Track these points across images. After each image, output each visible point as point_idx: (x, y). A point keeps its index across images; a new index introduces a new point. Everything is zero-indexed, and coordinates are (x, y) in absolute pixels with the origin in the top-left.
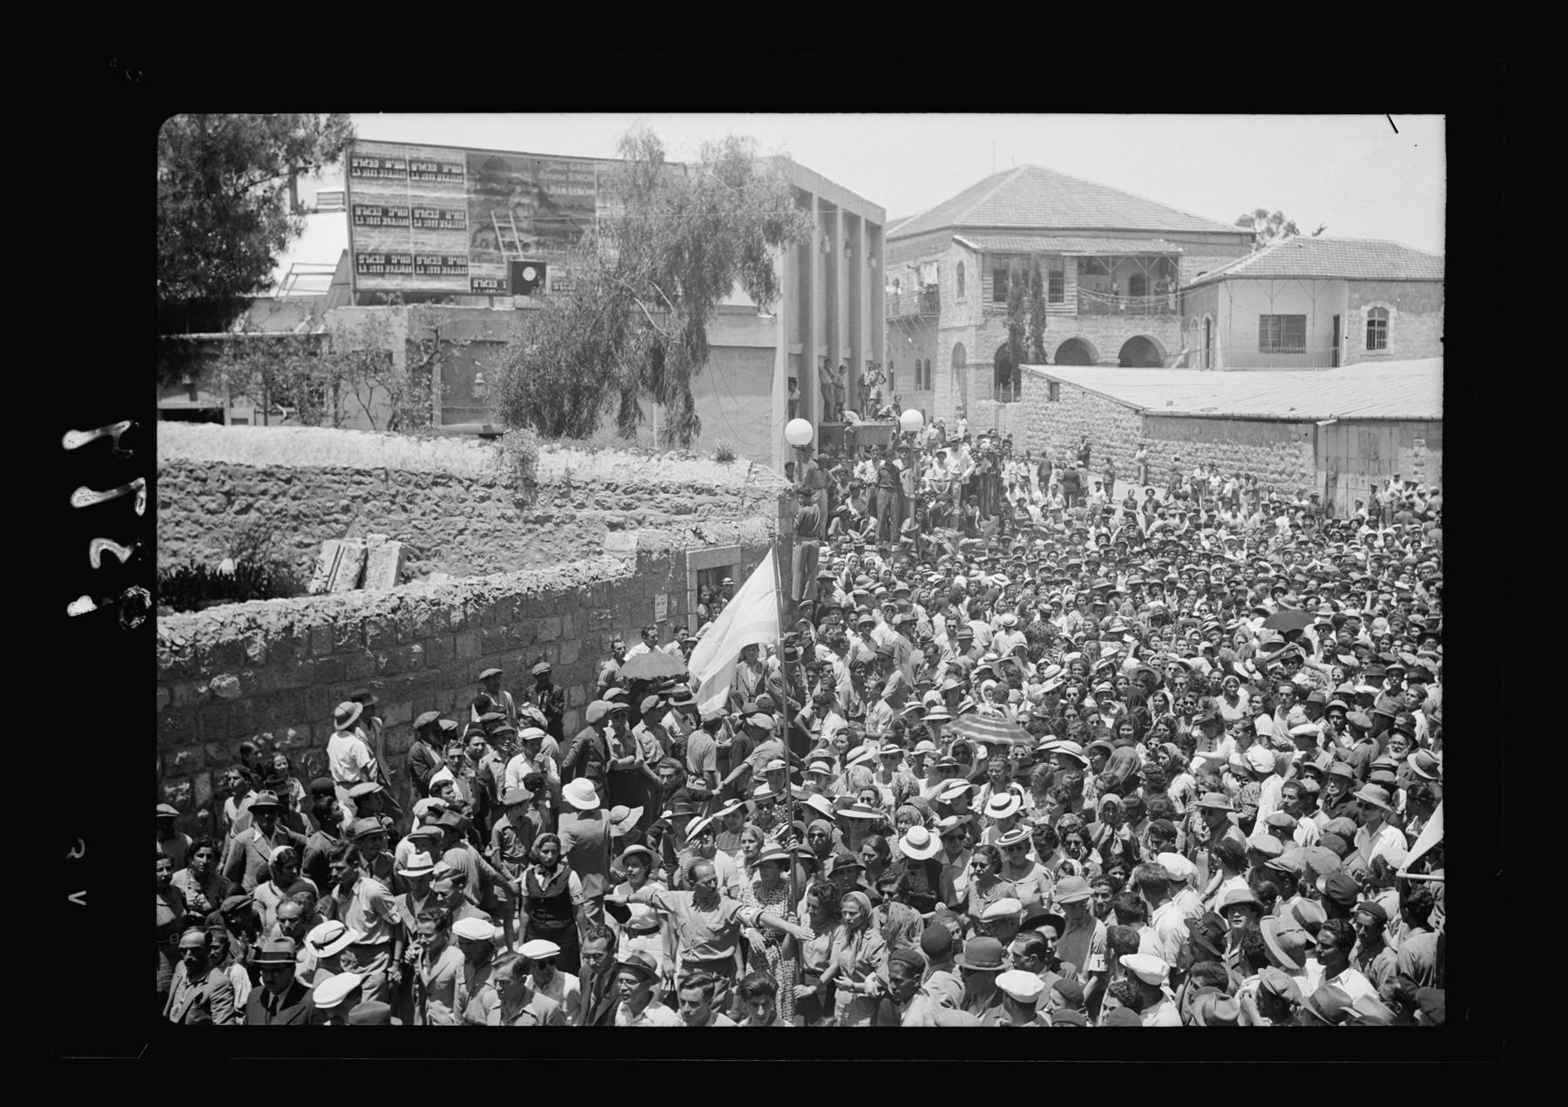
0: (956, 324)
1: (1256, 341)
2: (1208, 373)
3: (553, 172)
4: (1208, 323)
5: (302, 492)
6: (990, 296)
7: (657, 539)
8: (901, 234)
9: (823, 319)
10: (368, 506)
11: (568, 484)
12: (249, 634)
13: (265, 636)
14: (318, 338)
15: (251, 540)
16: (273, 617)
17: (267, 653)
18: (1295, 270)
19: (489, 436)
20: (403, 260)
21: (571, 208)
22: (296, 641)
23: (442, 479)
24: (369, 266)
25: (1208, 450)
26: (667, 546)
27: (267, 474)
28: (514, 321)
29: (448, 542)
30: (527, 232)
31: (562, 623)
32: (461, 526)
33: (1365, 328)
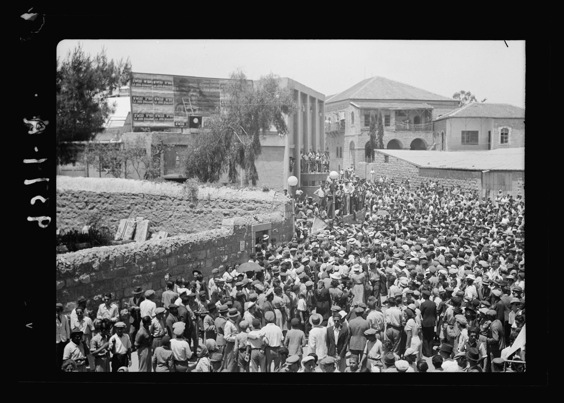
0: (350, 134)
1: (460, 140)
2: (443, 152)
3: (205, 83)
4: (443, 134)
5: (113, 202)
6: (363, 124)
7: (241, 220)
8: (331, 101)
9: (302, 135)
10: (137, 207)
11: (209, 200)
12: (93, 260)
13: (99, 261)
14: (119, 144)
15: (94, 220)
16: (102, 253)
17: (100, 266)
18: (474, 115)
19: (180, 181)
20: (150, 116)
21: (211, 96)
22: (111, 262)
23: (163, 197)
24: (138, 118)
25: (443, 181)
26: (244, 223)
27: (101, 195)
28: (190, 137)
29: (166, 220)
30: (195, 105)
31: (206, 252)
32: (170, 214)
33: (500, 136)
